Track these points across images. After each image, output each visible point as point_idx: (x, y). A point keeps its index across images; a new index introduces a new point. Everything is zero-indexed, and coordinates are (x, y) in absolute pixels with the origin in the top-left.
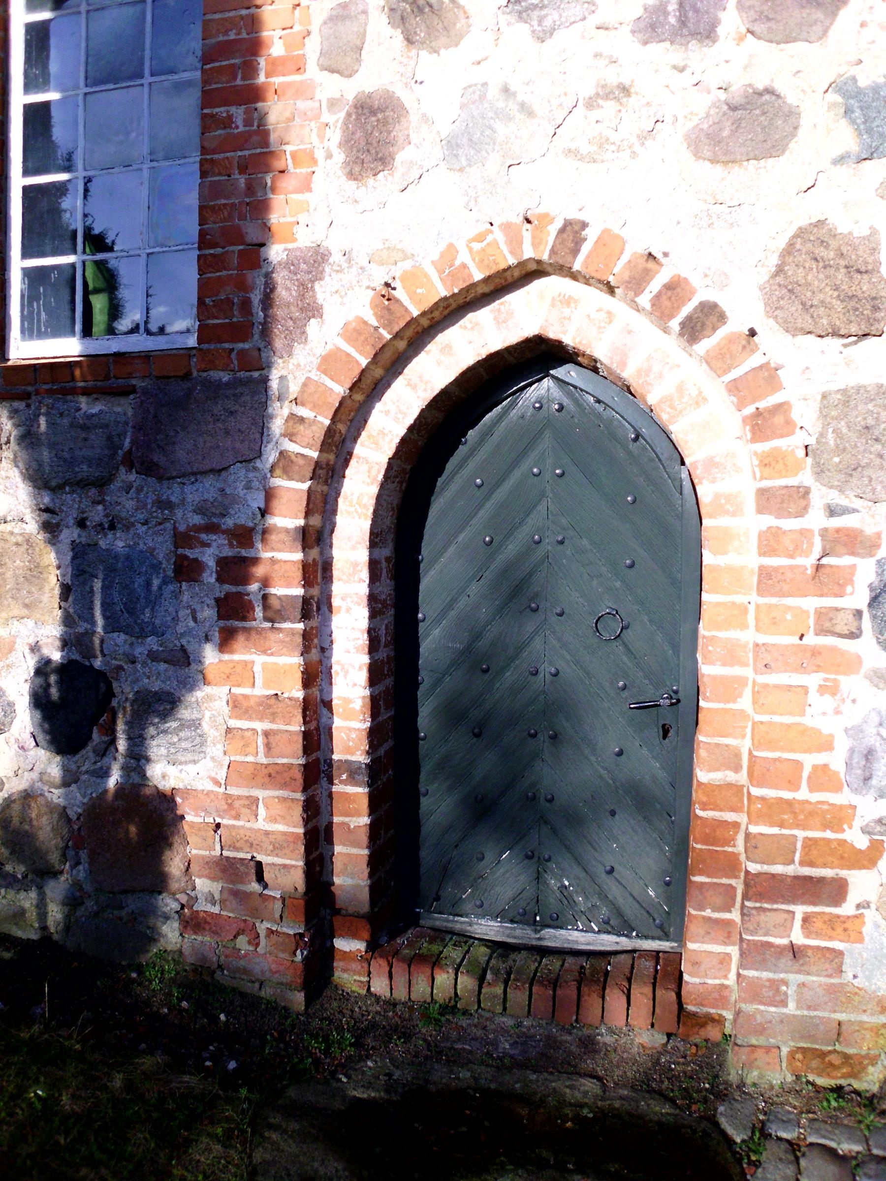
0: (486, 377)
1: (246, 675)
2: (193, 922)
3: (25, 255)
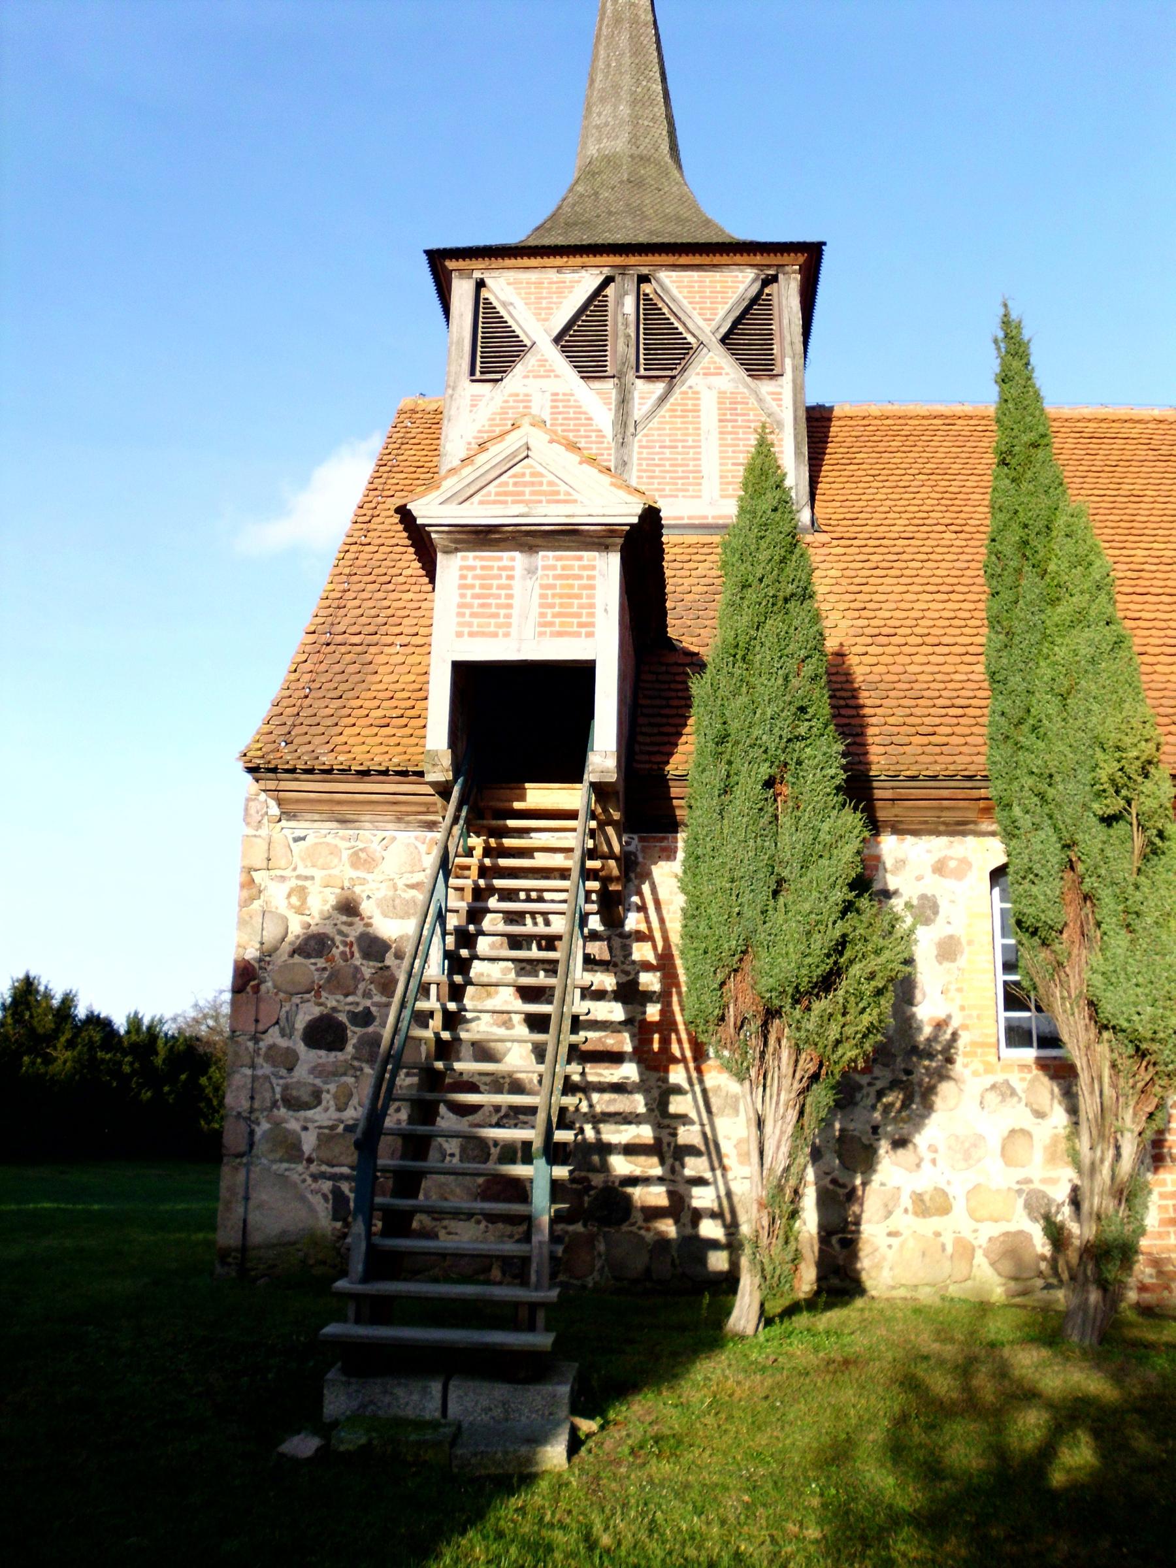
0: (55, 1003)
1: (1163, 1183)
2: (1143, 1288)
3: (584, 672)
